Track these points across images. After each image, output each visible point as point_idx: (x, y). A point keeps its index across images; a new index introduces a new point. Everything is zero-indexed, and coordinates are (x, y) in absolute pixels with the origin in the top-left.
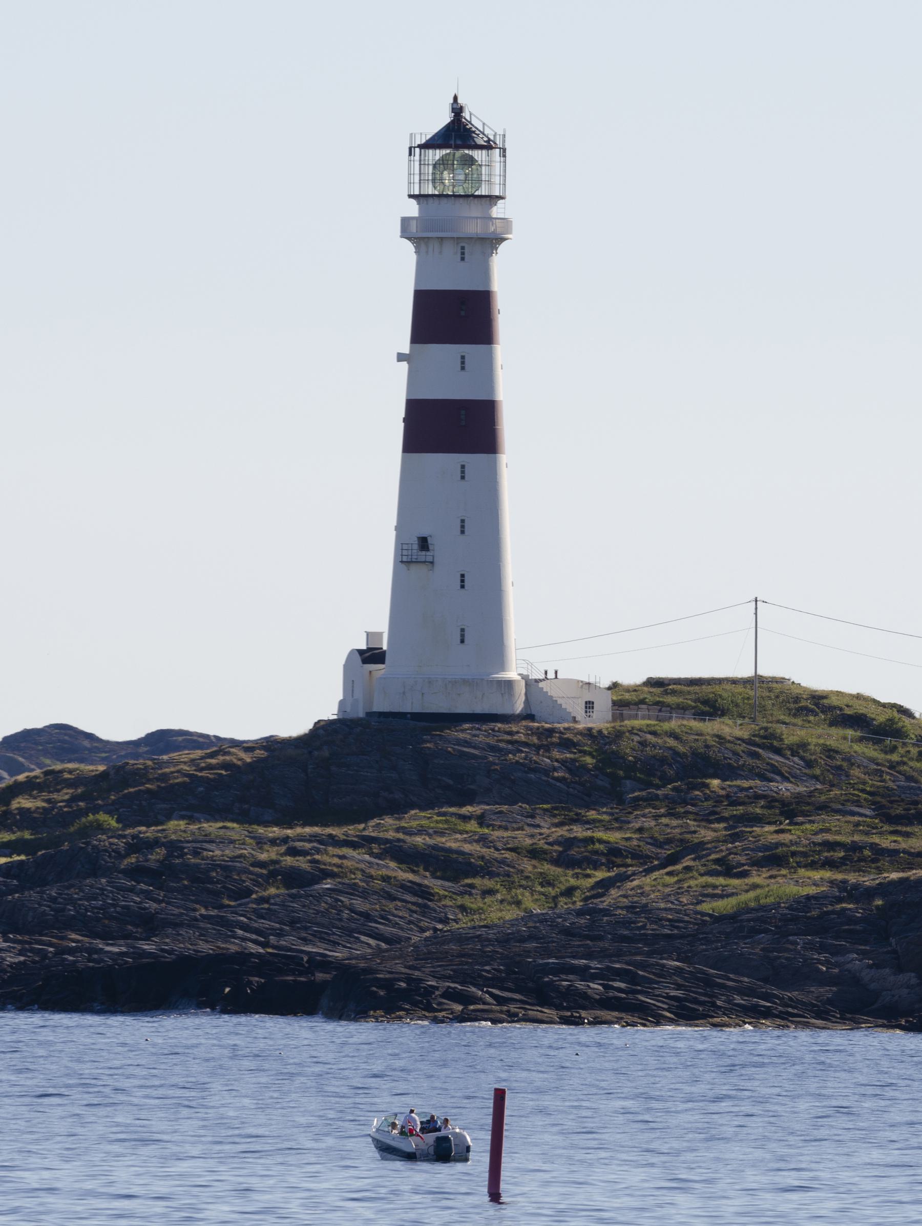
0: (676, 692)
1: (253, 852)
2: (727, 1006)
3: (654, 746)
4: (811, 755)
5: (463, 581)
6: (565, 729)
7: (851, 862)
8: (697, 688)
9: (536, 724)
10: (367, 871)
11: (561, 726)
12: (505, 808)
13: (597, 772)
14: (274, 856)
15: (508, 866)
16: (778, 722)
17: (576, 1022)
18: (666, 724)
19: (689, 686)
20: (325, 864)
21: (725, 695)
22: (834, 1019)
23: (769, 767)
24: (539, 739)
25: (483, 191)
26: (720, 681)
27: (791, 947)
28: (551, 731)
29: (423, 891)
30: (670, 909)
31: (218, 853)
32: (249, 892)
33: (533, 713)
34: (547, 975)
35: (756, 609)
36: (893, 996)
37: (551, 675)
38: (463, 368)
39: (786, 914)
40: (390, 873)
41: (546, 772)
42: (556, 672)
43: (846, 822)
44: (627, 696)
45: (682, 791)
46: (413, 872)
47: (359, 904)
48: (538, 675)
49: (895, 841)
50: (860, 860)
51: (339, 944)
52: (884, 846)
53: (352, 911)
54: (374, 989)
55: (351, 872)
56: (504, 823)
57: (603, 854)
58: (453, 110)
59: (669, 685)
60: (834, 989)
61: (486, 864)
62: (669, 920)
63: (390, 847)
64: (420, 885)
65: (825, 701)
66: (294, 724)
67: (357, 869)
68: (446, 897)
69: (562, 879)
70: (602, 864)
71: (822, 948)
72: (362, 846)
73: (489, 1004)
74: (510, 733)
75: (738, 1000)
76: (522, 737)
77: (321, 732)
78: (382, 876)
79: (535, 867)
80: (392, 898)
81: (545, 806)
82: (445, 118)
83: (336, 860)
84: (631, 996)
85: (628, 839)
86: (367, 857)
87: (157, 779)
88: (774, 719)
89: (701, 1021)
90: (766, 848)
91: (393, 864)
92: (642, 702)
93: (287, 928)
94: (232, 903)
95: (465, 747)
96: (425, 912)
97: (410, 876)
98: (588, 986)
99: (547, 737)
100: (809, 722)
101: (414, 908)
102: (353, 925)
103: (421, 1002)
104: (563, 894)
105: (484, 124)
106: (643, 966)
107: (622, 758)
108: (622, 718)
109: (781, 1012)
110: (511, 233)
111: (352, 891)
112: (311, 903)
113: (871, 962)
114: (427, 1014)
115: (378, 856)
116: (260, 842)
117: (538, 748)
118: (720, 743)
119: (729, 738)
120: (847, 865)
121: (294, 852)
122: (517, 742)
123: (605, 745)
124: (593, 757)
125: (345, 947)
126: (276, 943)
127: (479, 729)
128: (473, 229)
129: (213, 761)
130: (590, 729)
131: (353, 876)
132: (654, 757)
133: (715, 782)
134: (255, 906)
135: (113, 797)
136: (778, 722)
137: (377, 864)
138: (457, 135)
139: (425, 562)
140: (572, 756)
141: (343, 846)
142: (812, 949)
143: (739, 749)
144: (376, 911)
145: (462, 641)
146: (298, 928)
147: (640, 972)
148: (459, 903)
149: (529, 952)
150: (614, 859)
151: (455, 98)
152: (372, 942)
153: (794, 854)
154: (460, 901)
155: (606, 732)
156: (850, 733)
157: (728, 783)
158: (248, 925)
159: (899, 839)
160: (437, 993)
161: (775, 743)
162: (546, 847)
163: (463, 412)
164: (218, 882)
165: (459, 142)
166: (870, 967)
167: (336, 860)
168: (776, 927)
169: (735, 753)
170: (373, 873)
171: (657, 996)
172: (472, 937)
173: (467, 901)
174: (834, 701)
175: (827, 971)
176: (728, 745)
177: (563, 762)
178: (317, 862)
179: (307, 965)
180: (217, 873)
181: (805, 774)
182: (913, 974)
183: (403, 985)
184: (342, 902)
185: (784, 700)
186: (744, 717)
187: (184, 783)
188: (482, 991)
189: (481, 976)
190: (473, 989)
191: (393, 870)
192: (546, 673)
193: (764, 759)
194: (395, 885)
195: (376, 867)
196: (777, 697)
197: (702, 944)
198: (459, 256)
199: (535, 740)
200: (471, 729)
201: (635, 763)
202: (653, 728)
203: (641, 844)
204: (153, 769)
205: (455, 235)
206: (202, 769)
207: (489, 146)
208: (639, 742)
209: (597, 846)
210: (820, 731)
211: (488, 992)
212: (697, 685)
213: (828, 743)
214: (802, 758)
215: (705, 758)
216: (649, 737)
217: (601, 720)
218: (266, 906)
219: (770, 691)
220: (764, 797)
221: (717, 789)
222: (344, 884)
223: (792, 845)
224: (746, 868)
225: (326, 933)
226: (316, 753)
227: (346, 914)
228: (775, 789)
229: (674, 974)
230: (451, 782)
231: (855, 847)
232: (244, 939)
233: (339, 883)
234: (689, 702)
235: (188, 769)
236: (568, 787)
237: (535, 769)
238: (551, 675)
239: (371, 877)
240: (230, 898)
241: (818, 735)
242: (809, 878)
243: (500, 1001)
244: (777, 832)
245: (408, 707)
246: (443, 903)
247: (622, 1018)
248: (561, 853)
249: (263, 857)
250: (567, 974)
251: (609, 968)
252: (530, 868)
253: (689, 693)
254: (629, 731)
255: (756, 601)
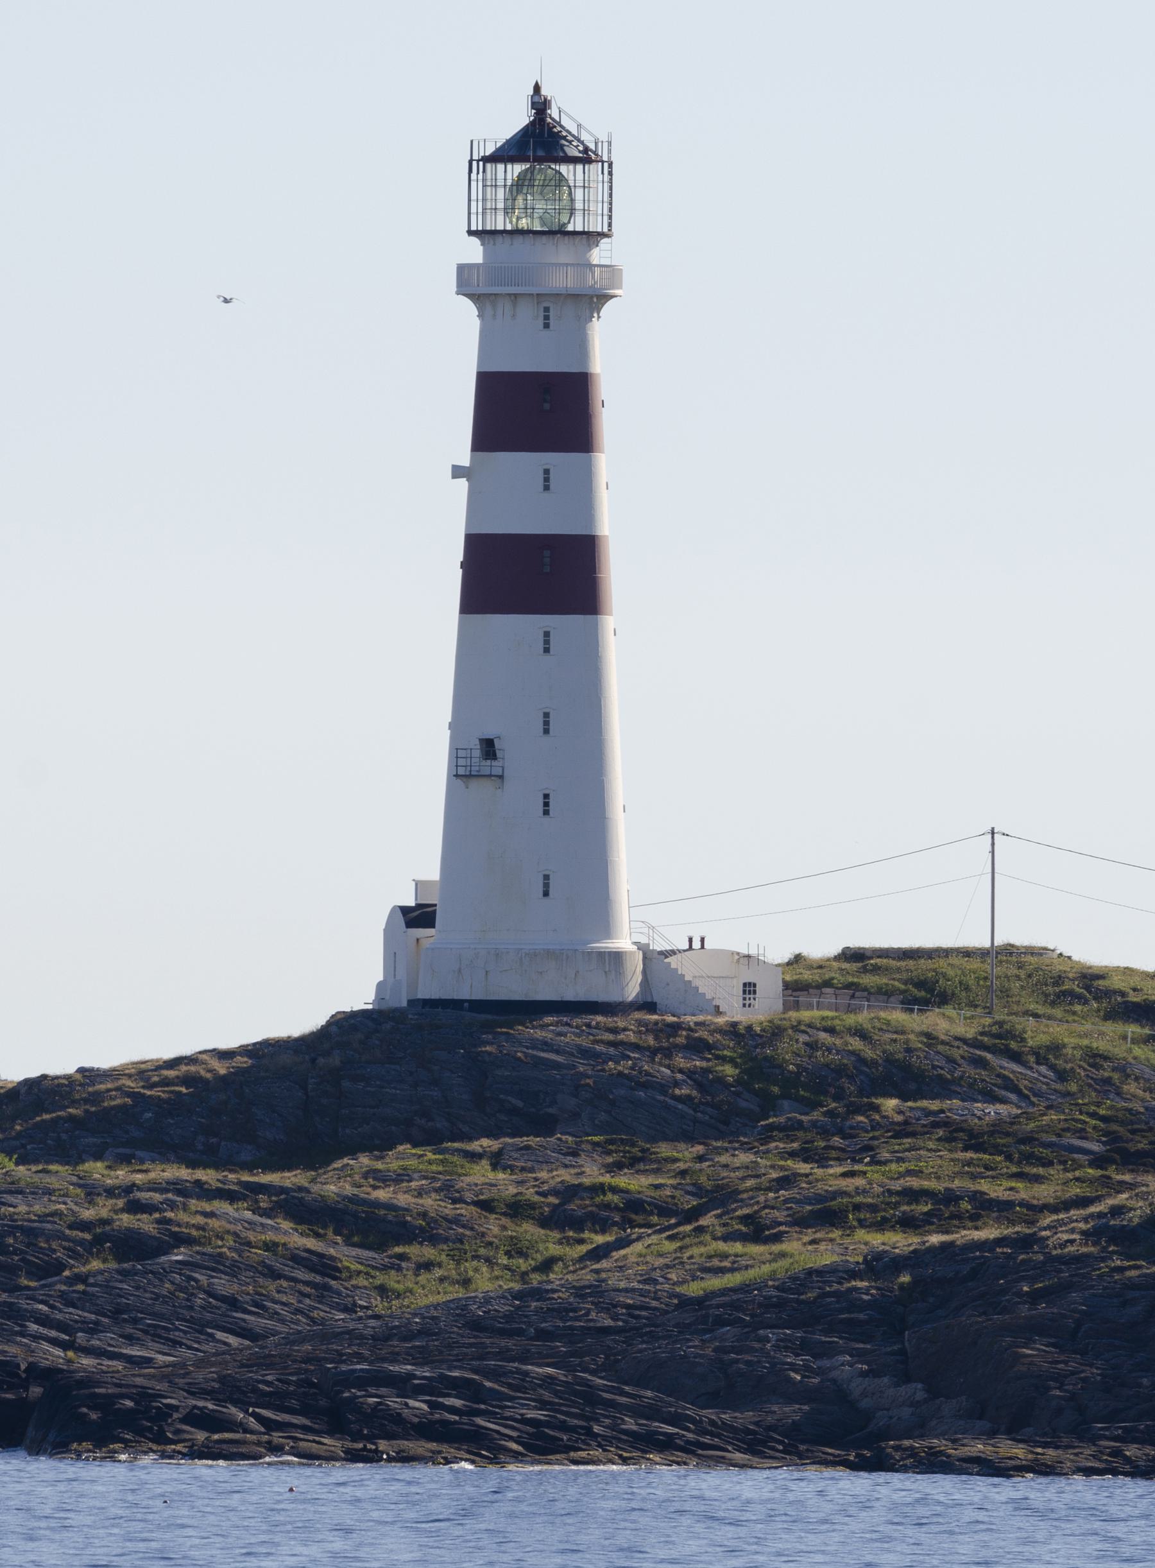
0: (879, 968)
1: (74, 1208)
2: (609, 1433)
3: (829, 1050)
4: (1066, 1062)
5: (546, 804)
6: (696, 1024)
7: (940, 1220)
8: (911, 962)
9: (655, 1017)
10: (243, 1235)
11: (690, 1019)
12: (533, 1141)
13: (740, 1089)
14: (104, 1213)
15: (464, 1226)
16: (1027, 1013)
17: (371, 1458)
18: (852, 1016)
19: (900, 959)
20: (179, 1225)
21: (951, 973)
22: (771, 1453)
23: (999, 1081)
24: (656, 1038)
25: (576, 224)
26: (946, 953)
27: (757, 1345)
28: (675, 1028)
29: (325, 1265)
30: (633, 1290)
31: (23, 1208)
32: (60, 1267)
33: (655, 999)
34: (348, 1388)
35: (993, 844)
36: (891, 1418)
37: (696, 945)
38: (547, 488)
39: (771, 1297)
40: (280, 1239)
41: (663, 1088)
42: (702, 940)
43: (952, 1160)
44: (807, 976)
45: (838, 1115)
46: (317, 1235)
47: (223, 1284)
48: (659, 945)
49: (1011, 1189)
50: (953, 1217)
51: (181, 1344)
52: (993, 1195)
53: (210, 1294)
54: (85, 1410)
55: (217, 1237)
56: (529, 1164)
57: (617, 1208)
58: (534, 105)
59: (871, 958)
60: (806, 1407)
61: (428, 1224)
62: (628, 1307)
63: (285, 1199)
64: (321, 1256)
65: (1101, 982)
66: (299, 1016)
67: (228, 1232)
68: (359, 1273)
69: (541, 1247)
70: (615, 1224)
71: (804, 1347)
72: (244, 1198)
73: (252, 1432)
74: (614, 1031)
75: (630, 1424)
76: (632, 1037)
77: (334, 1029)
78: (265, 1243)
79: (504, 1228)
80: (275, 1275)
81: (596, 1139)
82: (520, 118)
83: (200, 1220)
84: (465, 1419)
85: (657, 1187)
86: (248, 1215)
87: (85, 1101)
88: (1020, 1009)
89: (558, 1456)
90: (819, 1199)
91: (286, 1225)
92: (828, 983)
93: (107, 1320)
94: (33, 1284)
95: (544, 1051)
96: (323, 1296)
97: (311, 1243)
98: (406, 1404)
99: (669, 1036)
100: (1074, 1013)
101: (308, 1290)
102: (208, 1316)
103: (150, 1429)
104: (535, 1269)
105: (579, 126)
106: (495, 1374)
107: (780, 1066)
108: (797, 1006)
109: (688, 1442)
110: (621, 288)
111: (217, 1263)
112: (150, 1282)
113: (865, 1367)
114: (155, 1447)
115: (265, 1213)
116: (91, 1192)
117: (654, 1052)
118: (929, 1046)
119: (943, 1037)
120: (932, 1224)
121: (135, 1207)
122: (622, 1043)
123: (756, 1047)
124: (736, 1065)
125: (189, 1348)
126: (84, 1343)
127: (567, 1024)
128: (562, 281)
129: (171, 1073)
130: (734, 1025)
131: (220, 1243)
132: (827, 1065)
133: (891, 1103)
134: (63, 1288)
135: (18, 1128)
136: (1027, 1013)
137: (262, 1225)
138: (540, 143)
139: (490, 776)
140: (704, 1064)
141: (215, 1198)
142: (786, 1348)
143: (956, 1054)
144: (248, 1294)
145: (546, 894)
146: (125, 1320)
147: (488, 1384)
148: (378, 1282)
149: (398, 1354)
150: (633, 1216)
151: (537, 88)
152: (233, 1340)
153: (857, 1207)
154: (380, 1279)
155: (758, 1029)
156: (1133, 1029)
157: (910, 1104)
158: (47, 1316)
159: (1020, 1185)
160: (176, 1415)
161: (1013, 1045)
162: (537, 1198)
163: (547, 553)
164: (15, 1253)
165: (540, 153)
166: (863, 1374)
167: (200, 1220)
168: (752, 1316)
169: (951, 1060)
170: (252, 1239)
171: (507, 1419)
172: (343, 1333)
173: (391, 1280)
174: (1116, 983)
175: (800, 1382)
176: (940, 1048)
177: (690, 1074)
178: (169, 1221)
179: (24, 1375)
180: (15, 1238)
181: (1055, 1090)
182: (920, 1386)
183: (129, 1403)
184: (196, 1281)
185: (1038, 981)
186: (976, 1006)
187: (125, 1105)
188: (246, 1412)
189: (255, 1390)
190: (233, 1410)
191: (286, 1233)
192: (691, 940)
193: (992, 1069)
194: (283, 1256)
195: (259, 1229)
196: (1030, 976)
197: (643, 1342)
198: (541, 321)
199: (651, 1041)
200: (557, 1024)
201: (798, 1074)
202: (829, 1023)
203: (678, 1193)
204: (80, 1085)
205: (534, 290)
206: (152, 1086)
207: (586, 158)
208: (806, 1044)
209: (610, 1197)
210: (1088, 1026)
211: (254, 1415)
212: (911, 958)
213: (1095, 1045)
214: (1052, 1067)
215: (905, 1068)
216: (823, 1035)
217: (767, 1007)
218: (81, 1287)
219: (1019, 968)
220: (946, 1124)
221: (890, 1113)
222: (204, 1254)
223: (858, 1194)
224: (783, 1228)
225: (164, 1328)
226: (321, 1061)
227: (200, 1300)
228: (979, 1113)
229: (540, 1386)
230: (520, 1104)
231: (951, 1198)
232: (36, 1337)
233: (198, 1253)
234: (896, 983)
235: (132, 1085)
236: (695, 1110)
237: (647, 1084)
238: (696, 945)
239: (249, 1244)
240: (30, 1275)
241: (1081, 1032)
242: (866, 1244)
243: (270, 1425)
244: (845, 1175)
245: (466, 991)
246: (354, 1282)
247: (440, 1452)
248: (555, 1208)
249: (88, 1214)
250: (378, 1386)
251: (443, 1378)
252: (496, 1230)
253: (899, 970)
254: (793, 1027)
255: (993, 833)
